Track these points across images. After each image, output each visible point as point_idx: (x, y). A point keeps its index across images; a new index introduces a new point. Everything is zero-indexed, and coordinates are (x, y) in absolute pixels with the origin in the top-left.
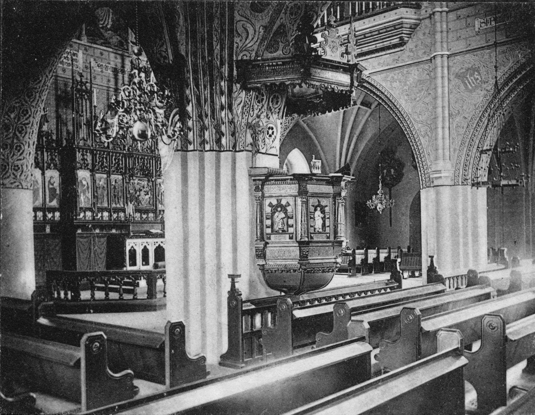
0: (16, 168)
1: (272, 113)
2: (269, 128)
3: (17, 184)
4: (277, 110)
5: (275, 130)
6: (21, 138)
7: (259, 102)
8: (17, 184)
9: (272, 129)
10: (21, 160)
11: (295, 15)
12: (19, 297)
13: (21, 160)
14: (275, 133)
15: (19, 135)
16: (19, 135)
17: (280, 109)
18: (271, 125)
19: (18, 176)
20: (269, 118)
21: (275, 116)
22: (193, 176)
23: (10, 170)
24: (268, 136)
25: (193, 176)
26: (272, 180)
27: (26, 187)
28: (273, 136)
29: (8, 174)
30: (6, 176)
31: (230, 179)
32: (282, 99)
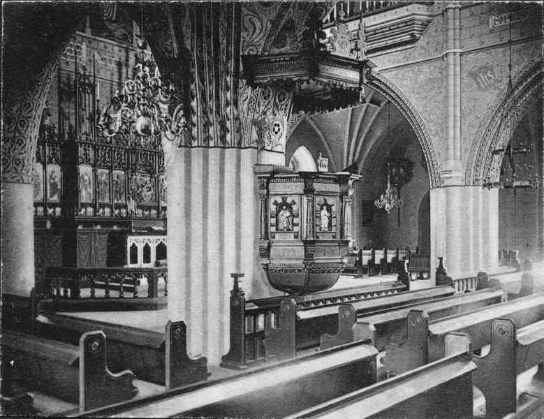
7: (265, 98)
9: (278, 126)
10: (22, 154)
13: (22, 154)
14: (281, 131)
15: (21, 128)
16: (21, 128)
17: (286, 106)
18: (277, 122)
20: (275, 115)
21: (282, 113)
26: (278, 178)
28: (279, 134)
29: (9, 169)
30: (7, 170)
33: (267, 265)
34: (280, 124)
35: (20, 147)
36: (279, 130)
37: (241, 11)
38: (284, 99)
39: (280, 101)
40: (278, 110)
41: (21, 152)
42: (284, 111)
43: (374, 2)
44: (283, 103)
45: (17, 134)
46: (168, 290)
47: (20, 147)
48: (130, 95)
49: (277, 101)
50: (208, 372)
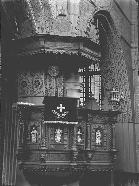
2: (36, 82)
14: (41, 83)
18: (36, 80)
27: (126, 121)
41: (112, 67)
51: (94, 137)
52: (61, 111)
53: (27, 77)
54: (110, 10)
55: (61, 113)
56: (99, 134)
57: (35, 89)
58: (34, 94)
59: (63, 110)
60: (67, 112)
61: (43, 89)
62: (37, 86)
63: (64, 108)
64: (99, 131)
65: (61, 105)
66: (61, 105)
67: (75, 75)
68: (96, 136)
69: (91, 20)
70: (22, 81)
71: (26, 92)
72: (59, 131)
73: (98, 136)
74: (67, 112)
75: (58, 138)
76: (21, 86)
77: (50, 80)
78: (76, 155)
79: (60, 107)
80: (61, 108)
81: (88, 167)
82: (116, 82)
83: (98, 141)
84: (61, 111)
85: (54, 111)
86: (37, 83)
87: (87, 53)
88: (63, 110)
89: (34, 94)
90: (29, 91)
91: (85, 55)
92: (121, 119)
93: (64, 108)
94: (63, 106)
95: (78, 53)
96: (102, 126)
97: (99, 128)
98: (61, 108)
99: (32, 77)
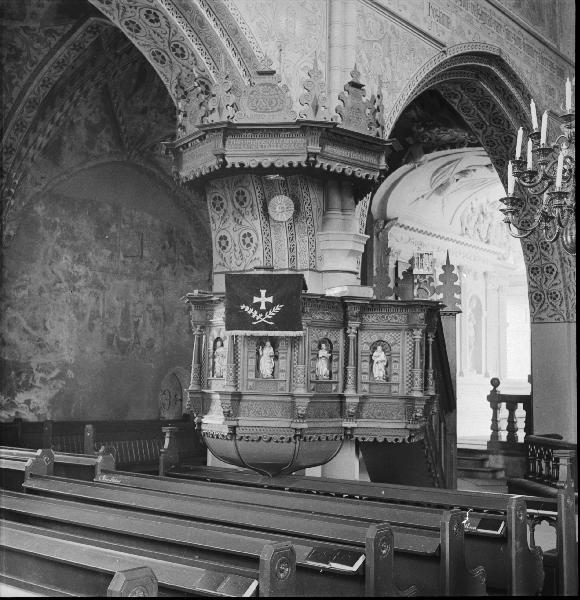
0: (554, 296)
1: (243, 216)
2: (245, 236)
3: (557, 317)
4: (249, 209)
5: (254, 236)
6: (550, 257)
7: (218, 209)
8: (557, 317)
9: (249, 235)
11: (124, 262)
12: (470, 480)
14: (255, 240)
17: (252, 206)
18: (246, 232)
19: (558, 307)
21: (249, 217)
22: (190, 233)
23: (546, 301)
24: (245, 247)
25: (190, 233)
26: (249, 401)
28: (253, 245)
29: (545, 306)
31: (134, 531)
32: (249, 192)
33: (79, 261)
34: (251, 232)
35: (553, 276)
36: (174, 50)
37: (76, 357)
38: (245, 199)
39: (241, 204)
40: (243, 216)
42: (251, 214)
43: (441, 296)
44: (245, 204)
45: (544, 262)
46: (430, 237)
47: (553, 276)
48: (90, 115)
49: (237, 205)
50: (287, 166)
51: (367, 364)
52: (263, 307)
53: (226, 225)
54: (504, 50)
55: (263, 312)
56: (380, 356)
57: (245, 253)
58: (243, 264)
59: (259, 304)
60: (277, 308)
61: (260, 254)
62: (248, 245)
63: (270, 299)
64: (323, 346)
65: (263, 292)
66: (263, 292)
67: (342, 217)
68: (372, 361)
69: (185, 116)
70: (219, 235)
71: (228, 261)
72: (268, 350)
73: (378, 359)
74: (277, 308)
75: (266, 366)
76: (219, 248)
77: (278, 231)
78: (302, 406)
79: (260, 296)
80: (263, 299)
81: (349, 433)
82: (257, 245)
83: (379, 372)
84: (263, 307)
85: (247, 309)
86: (247, 240)
87: (336, 160)
88: (259, 304)
89: (243, 264)
90: (234, 260)
91: (329, 167)
92: (565, 315)
93: (270, 299)
94: (267, 296)
95: (307, 162)
96: (388, 337)
97: (327, 341)
98: (263, 299)
99: (238, 227)
